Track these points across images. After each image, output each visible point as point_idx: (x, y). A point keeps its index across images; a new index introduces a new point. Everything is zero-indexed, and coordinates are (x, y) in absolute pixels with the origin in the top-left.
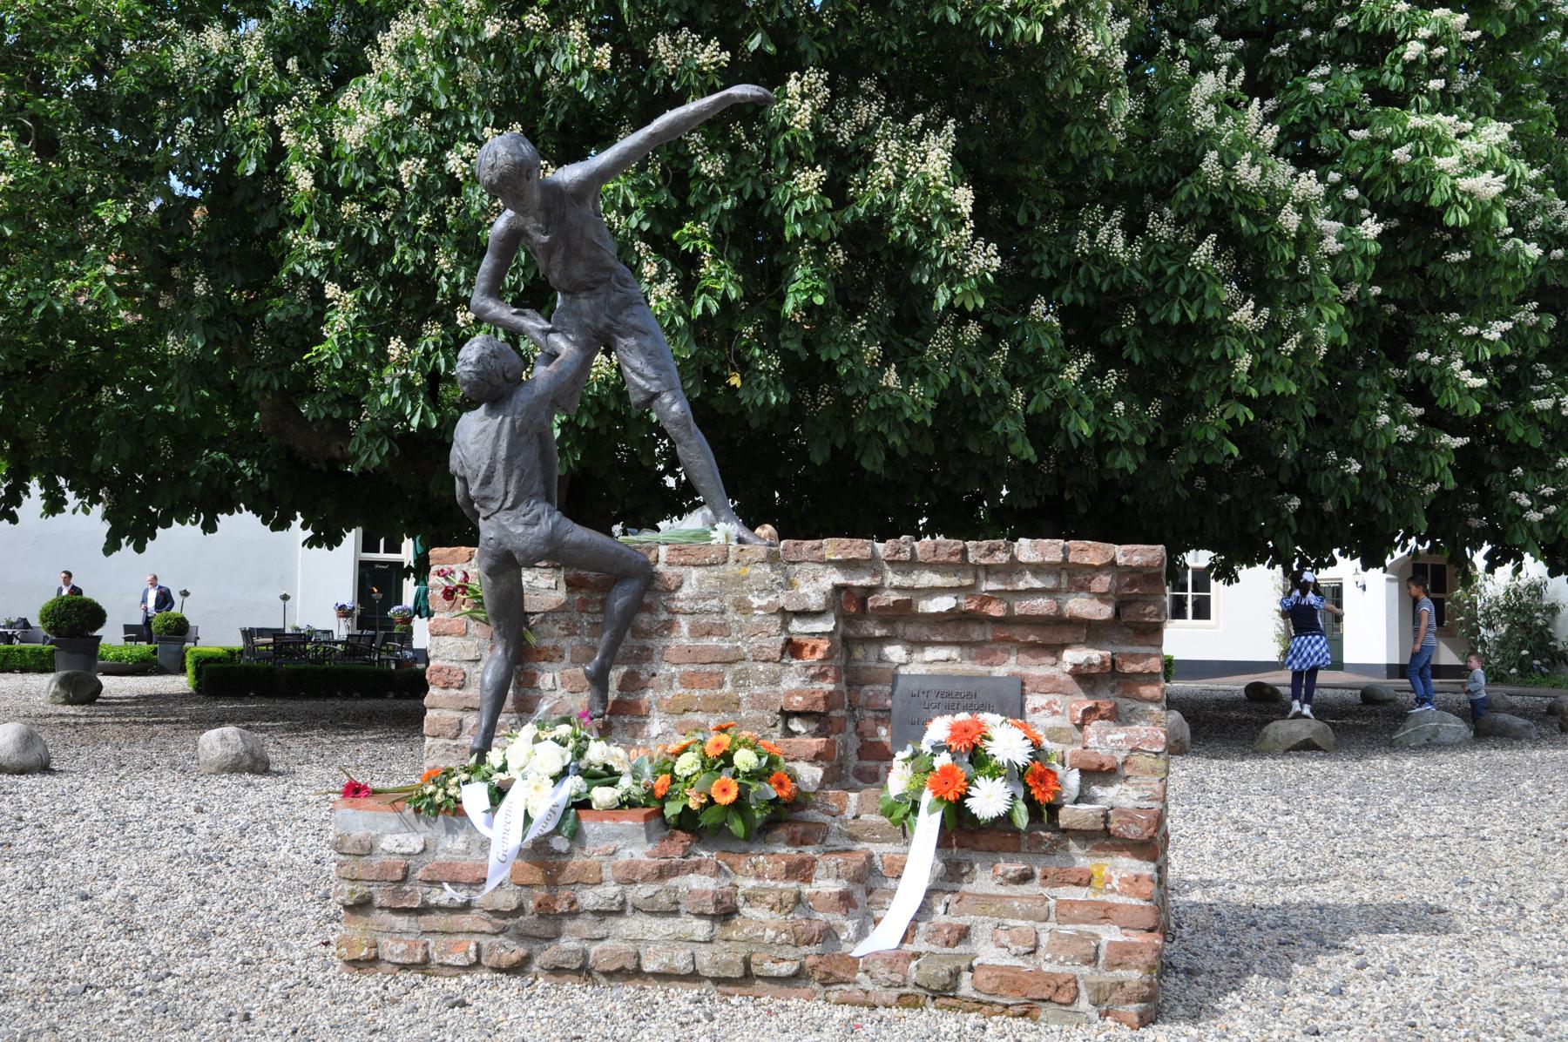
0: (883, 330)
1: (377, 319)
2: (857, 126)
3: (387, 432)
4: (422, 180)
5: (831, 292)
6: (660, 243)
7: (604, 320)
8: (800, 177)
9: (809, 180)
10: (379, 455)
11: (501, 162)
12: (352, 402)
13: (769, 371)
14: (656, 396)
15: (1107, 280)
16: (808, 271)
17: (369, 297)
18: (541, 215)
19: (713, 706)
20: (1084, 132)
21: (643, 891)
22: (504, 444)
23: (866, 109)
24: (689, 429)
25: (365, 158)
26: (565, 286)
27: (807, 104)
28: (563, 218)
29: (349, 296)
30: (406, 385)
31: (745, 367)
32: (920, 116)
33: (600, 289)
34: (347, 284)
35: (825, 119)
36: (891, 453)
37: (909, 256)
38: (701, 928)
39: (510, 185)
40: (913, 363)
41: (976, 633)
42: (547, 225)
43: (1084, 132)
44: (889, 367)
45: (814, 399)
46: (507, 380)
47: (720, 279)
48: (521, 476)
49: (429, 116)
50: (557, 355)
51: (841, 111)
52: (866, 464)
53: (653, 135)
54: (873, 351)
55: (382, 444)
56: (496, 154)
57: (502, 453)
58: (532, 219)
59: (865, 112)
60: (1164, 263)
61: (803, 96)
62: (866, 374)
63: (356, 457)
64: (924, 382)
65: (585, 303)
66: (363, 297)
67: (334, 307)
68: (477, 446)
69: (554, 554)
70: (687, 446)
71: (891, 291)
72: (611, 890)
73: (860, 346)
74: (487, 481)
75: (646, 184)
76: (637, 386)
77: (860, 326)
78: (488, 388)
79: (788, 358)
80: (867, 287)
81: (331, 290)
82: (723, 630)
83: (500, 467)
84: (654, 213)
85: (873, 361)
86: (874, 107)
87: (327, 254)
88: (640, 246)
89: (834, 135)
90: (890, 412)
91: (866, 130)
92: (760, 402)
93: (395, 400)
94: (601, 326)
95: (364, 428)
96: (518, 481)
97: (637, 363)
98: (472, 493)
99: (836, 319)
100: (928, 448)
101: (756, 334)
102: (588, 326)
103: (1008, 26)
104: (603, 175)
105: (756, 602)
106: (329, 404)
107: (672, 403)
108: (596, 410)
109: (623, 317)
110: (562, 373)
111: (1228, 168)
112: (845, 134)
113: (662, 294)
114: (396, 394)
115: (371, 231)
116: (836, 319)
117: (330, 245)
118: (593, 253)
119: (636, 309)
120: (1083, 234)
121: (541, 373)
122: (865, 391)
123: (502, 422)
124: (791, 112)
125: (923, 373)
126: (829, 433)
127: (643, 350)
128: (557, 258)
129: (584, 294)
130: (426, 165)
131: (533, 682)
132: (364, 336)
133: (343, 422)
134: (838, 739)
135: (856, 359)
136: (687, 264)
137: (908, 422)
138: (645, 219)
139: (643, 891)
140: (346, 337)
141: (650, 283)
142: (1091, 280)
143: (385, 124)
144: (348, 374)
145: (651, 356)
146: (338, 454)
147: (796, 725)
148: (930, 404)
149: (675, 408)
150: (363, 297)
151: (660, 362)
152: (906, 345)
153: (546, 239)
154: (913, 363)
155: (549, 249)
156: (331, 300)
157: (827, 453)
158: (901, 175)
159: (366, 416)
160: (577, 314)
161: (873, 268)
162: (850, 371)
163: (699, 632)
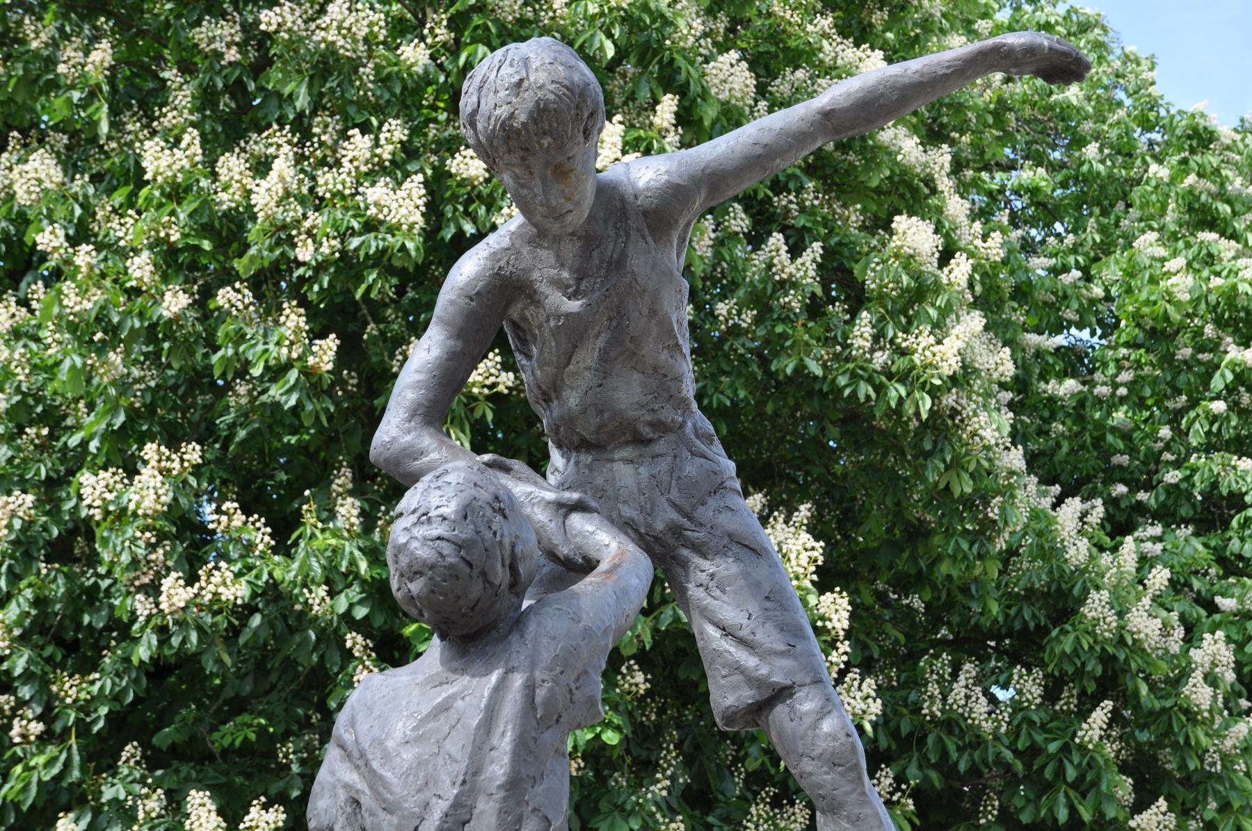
14: (782, 693)
15: (966, 757)
20: (965, 546)
22: (504, 741)
28: (618, 264)
33: (660, 447)
43: (965, 546)
57: (498, 769)
60: (1039, 738)
76: (738, 669)
88: (354, 640)
94: (659, 526)
97: (730, 614)
103: (880, 389)
111: (1120, 615)
120: (933, 689)
129: (627, 452)
138: (361, 602)
142: (945, 754)
153: (574, 306)
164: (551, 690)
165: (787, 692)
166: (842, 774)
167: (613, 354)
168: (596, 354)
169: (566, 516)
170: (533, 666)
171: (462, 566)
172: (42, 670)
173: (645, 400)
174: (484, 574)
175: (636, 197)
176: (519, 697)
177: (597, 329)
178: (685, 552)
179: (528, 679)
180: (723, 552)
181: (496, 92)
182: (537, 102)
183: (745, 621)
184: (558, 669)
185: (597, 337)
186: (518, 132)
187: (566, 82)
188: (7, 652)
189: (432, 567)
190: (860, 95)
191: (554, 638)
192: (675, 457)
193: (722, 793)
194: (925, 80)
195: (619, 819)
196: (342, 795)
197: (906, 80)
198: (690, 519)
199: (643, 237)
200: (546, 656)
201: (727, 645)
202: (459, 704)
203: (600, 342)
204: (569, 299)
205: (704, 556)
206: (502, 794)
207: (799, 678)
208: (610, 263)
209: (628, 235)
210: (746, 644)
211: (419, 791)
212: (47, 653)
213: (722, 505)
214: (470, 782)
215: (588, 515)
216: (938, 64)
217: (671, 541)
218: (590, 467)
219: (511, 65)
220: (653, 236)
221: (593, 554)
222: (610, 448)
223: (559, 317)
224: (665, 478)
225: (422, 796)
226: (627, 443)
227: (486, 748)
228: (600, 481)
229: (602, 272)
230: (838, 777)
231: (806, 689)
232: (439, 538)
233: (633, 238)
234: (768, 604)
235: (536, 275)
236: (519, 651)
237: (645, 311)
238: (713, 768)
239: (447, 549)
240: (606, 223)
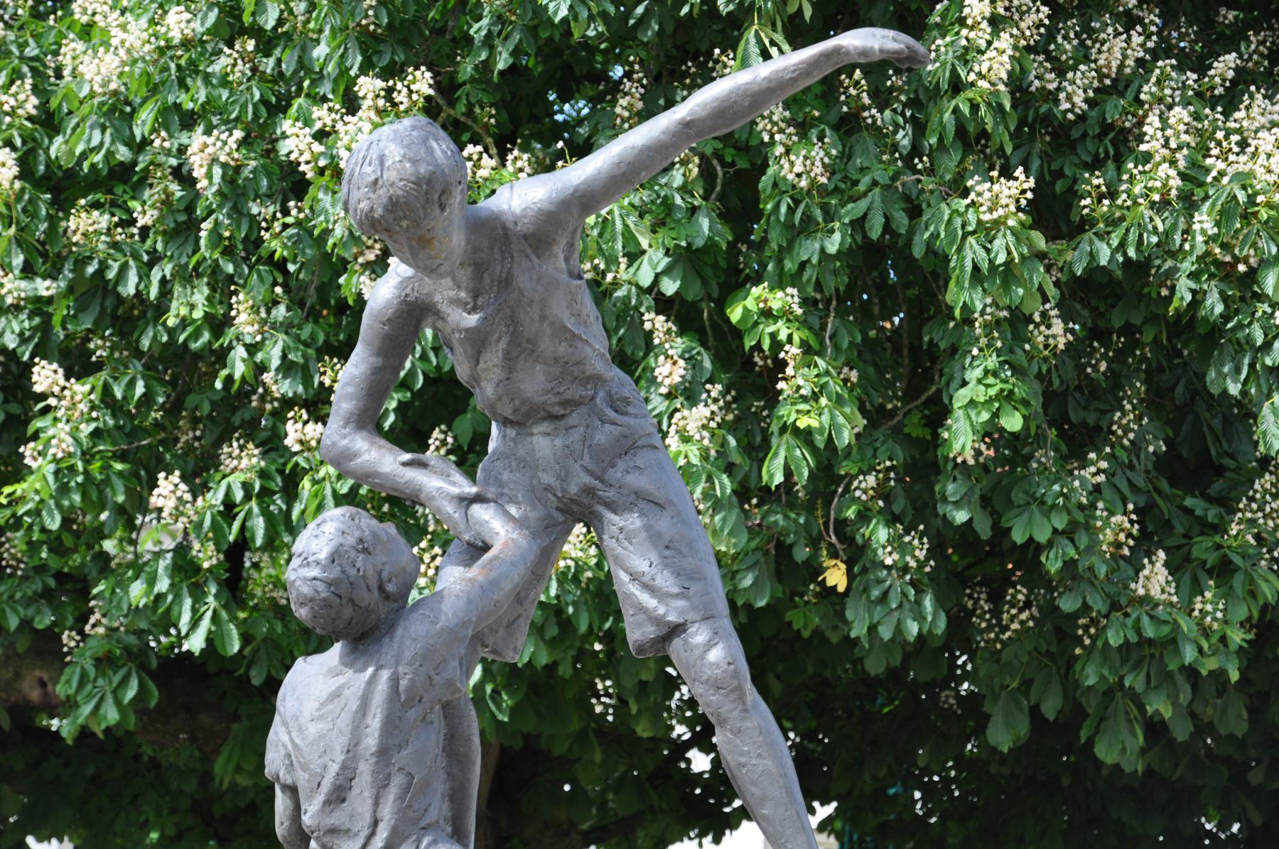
0: (1140, 481)
1: (134, 434)
2: (1101, 77)
3: (138, 657)
4: (232, 174)
5: (1037, 404)
6: (698, 317)
7: (580, 479)
8: (980, 188)
9: (1002, 196)
10: (118, 703)
11: (390, 175)
12: (72, 591)
13: (906, 569)
14: (676, 630)
16: (992, 362)
17: (118, 394)
18: (465, 275)
22: (375, 722)
23: (1120, 43)
24: (742, 697)
25: (118, 111)
26: (506, 410)
27: (1005, 41)
28: (506, 282)
29: (80, 388)
30: (184, 567)
31: (857, 555)
32: (1231, 58)
33: (574, 419)
34: (77, 364)
35: (1036, 64)
36: (1156, 729)
37: (1197, 338)
39: (404, 221)
40: (1202, 548)
42: (476, 295)
44: (1150, 554)
45: (996, 613)
46: (387, 597)
47: (816, 403)
48: (406, 789)
49: (251, 45)
50: (486, 547)
51: (1066, 47)
52: (1106, 752)
53: (687, 126)
54: (1116, 526)
55: (124, 681)
56: (382, 159)
57: (371, 741)
58: (448, 282)
59: (1118, 50)
61: (996, 22)
62: (1102, 570)
63: (70, 706)
64: (1226, 591)
65: (543, 443)
66: (107, 390)
67: (47, 410)
68: (322, 726)
70: (738, 732)
71: (1155, 403)
73: (1088, 511)
74: (338, 796)
75: (667, 204)
76: (641, 609)
77: (1094, 470)
78: (347, 612)
79: (944, 539)
80: (1105, 396)
81: (45, 376)
83: (365, 770)
84: (687, 259)
85: (1118, 545)
86: (1137, 40)
87: (39, 306)
88: (657, 323)
89: (1053, 97)
90: (1149, 653)
91: (1118, 86)
92: (886, 633)
93: (160, 597)
94: (573, 489)
95: (95, 647)
96: (401, 798)
98: (307, 820)
99: (1044, 457)
100: (1236, 722)
101: (882, 491)
102: (548, 488)
104: (586, 199)
106: (29, 601)
107: (709, 646)
108: (553, 631)
109: (615, 474)
110: (494, 583)
112: (1075, 94)
113: (692, 430)
114: (163, 585)
115: (123, 269)
116: (1044, 457)
117: (44, 287)
118: (562, 349)
119: (642, 459)
121: (453, 580)
122: (1098, 604)
123: (374, 677)
124: (967, 55)
125: (1224, 570)
126: (1027, 684)
127: (654, 537)
128: (493, 359)
129: (544, 427)
130: (242, 143)
132: (106, 468)
133: (51, 637)
135: (1083, 540)
136: (748, 379)
137: (1191, 673)
138: (667, 271)
140: (72, 469)
141: (670, 396)
143: (161, 51)
144: (68, 541)
145: (671, 551)
146: (35, 695)
148: (1237, 637)
149: (715, 655)
150: (107, 390)
151: (687, 563)
152: (1189, 512)
153: (472, 320)
154: (1202, 548)
155: (477, 341)
156: (43, 396)
157: (1023, 727)
158: (1193, 176)
159: (97, 626)
160: (527, 465)
161: (1121, 355)
162: (1070, 564)
164: (412, 680)
165: (681, 629)
166: (725, 696)
167: (514, 354)
168: (500, 354)
169: (467, 507)
170: (397, 663)
171: (333, 597)
172: (304, 356)
173: (549, 386)
174: (352, 601)
175: (516, 223)
176: (385, 687)
177: (496, 336)
178: (600, 509)
179: (393, 674)
180: (629, 508)
181: (359, 188)
182: (390, 198)
183: (646, 569)
184: (418, 664)
185: (498, 341)
186: (379, 221)
187: (412, 178)
188: (259, 338)
189: (311, 600)
190: (715, 104)
191: (415, 640)
192: (588, 426)
193: (1231, 456)
194: (773, 85)
195: (1037, 515)
196: (282, 752)
197: (756, 88)
198: (602, 481)
199: (527, 256)
200: (408, 655)
201: (635, 589)
202: (346, 692)
203: (502, 345)
204: (469, 313)
205: (615, 512)
206: (374, 759)
207: (691, 616)
208: (500, 282)
209: (512, 257)
210: (650, 588)
211: (320, 757)
212: (305, 334)
213: (631, 464)
214: (352, 750)
215: (485, 506)
216: (785, 69)
217: (586, 501)
218: (514, 440)
219: (370, 164)
220: (538, 257)
221: (488, 540)
222: (529, 423)
223: (460, 332)
224: (578, 447)
225: (321, 761)
226: (544, 419)
227: (363, 726)
228: (522, 453)
229: (495, 289)
230: (721, 698)
231: (696, 625)
232: (315, 579)
233: (516, 259)
234: (668, 553)
235: (437, 298)
236: (388, 651)
237: (536, 317)
238: (1217, 423)
239: (321, 586)
240: (491, 249)
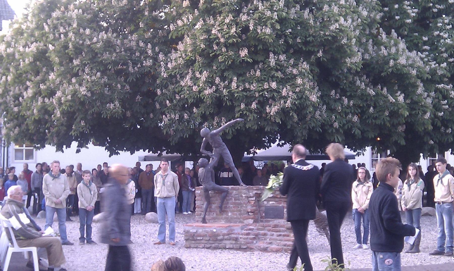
19: (237, 211)
21: (226, 237)
38: (234, 242)
41: (277, 200)
69: (214, 189)
72: (222, 237)
82: (239, 200)
105: (243, 195)
131: (409, 76)
134: (257, 216)
139: (226, 237)
147: (250, 214)
163: (235, 200)
